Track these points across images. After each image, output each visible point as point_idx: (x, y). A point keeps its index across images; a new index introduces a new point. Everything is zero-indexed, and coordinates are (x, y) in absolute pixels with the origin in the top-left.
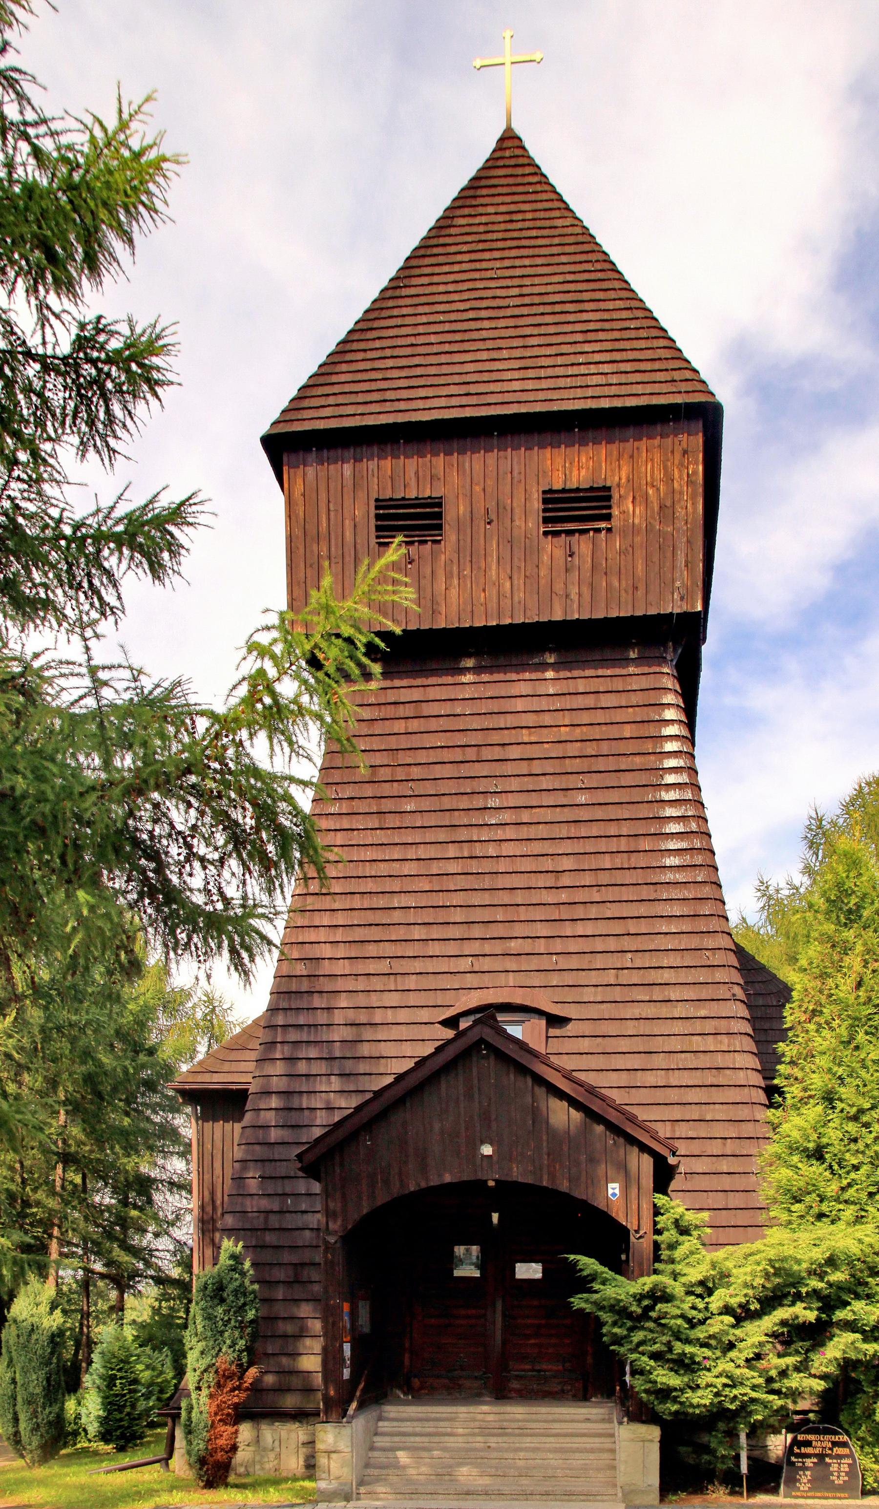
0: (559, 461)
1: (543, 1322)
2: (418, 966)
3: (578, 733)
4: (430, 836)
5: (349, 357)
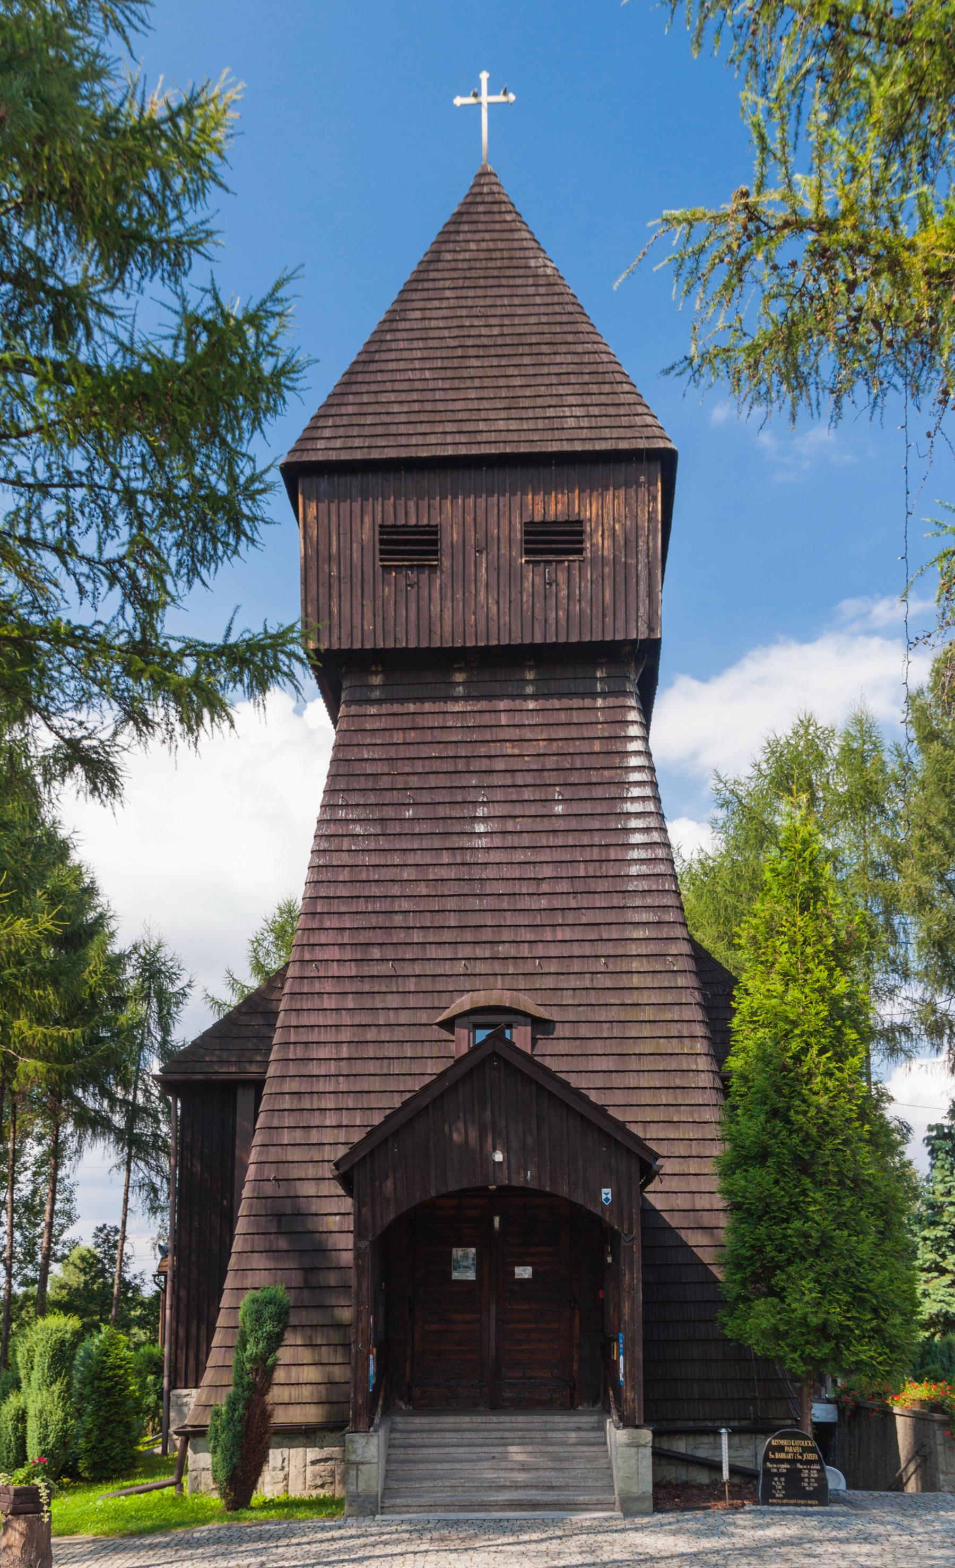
1: (532, 1326)
2: (418, 969)
3: (554, 747)
4: (426, 843)
5: (354, 388)
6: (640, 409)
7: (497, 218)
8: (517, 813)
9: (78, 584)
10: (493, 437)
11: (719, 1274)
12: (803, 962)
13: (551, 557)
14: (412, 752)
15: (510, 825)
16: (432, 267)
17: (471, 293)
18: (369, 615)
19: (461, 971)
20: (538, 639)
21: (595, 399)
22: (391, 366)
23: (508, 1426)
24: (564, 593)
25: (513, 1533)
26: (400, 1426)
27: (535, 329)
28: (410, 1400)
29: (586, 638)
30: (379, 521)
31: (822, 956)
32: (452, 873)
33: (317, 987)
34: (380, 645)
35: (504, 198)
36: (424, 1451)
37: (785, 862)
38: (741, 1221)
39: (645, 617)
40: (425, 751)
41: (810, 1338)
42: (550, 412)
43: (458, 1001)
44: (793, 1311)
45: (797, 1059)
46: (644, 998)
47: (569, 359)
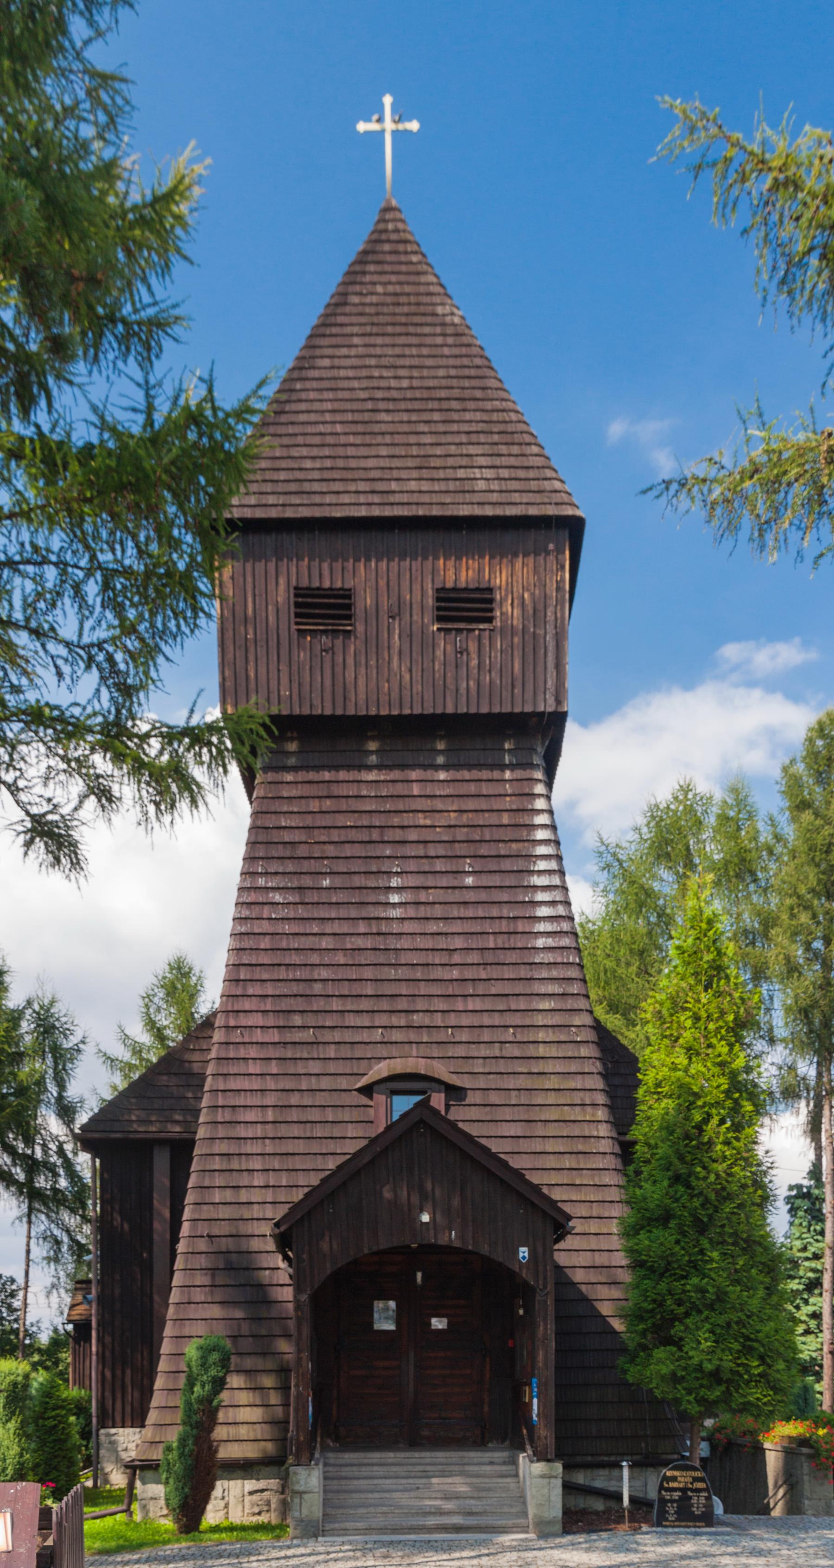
0: (451, 563)
2: (337, 1036)
3: (465, 819)
4: (343, 912)
6: (549, 473)
7: (403, 258)
8: (430, 884)
9: (56, 667)
10: (405, 498)
11: (618, 1325)
12: (706, 1037)
13: (462, 625)
14: (327, 820)
15: (423, 897)
16: (339, 310)
17: (379, 340)
18: (285, 680)
19: (379, 1039)
20: (450, 710)
21: (504, 461)
22: (302, 418)
23: (428, 1461)
24: (474, 662)
25: (444, 1551)
26: (332, 1461)
27: (444, 382)
28: (337, 1439)
29: (496, 710)
30: (294, 582)
31: (723, 1031)
32: (368, 943)
33: (242, 1053)
34: (297, 711)
35: (409, 237)
36: (355, 1482)
37: (690, 941)
38: (645, 1277)
39: (553, 690)
40: (341, 820)
41: (705, 1382)
42: (461, 473)
43: (376, 1068)
44: (690, 1358)
45: (699, 1128)
46: (550, 1067)
47: (478, 416)
